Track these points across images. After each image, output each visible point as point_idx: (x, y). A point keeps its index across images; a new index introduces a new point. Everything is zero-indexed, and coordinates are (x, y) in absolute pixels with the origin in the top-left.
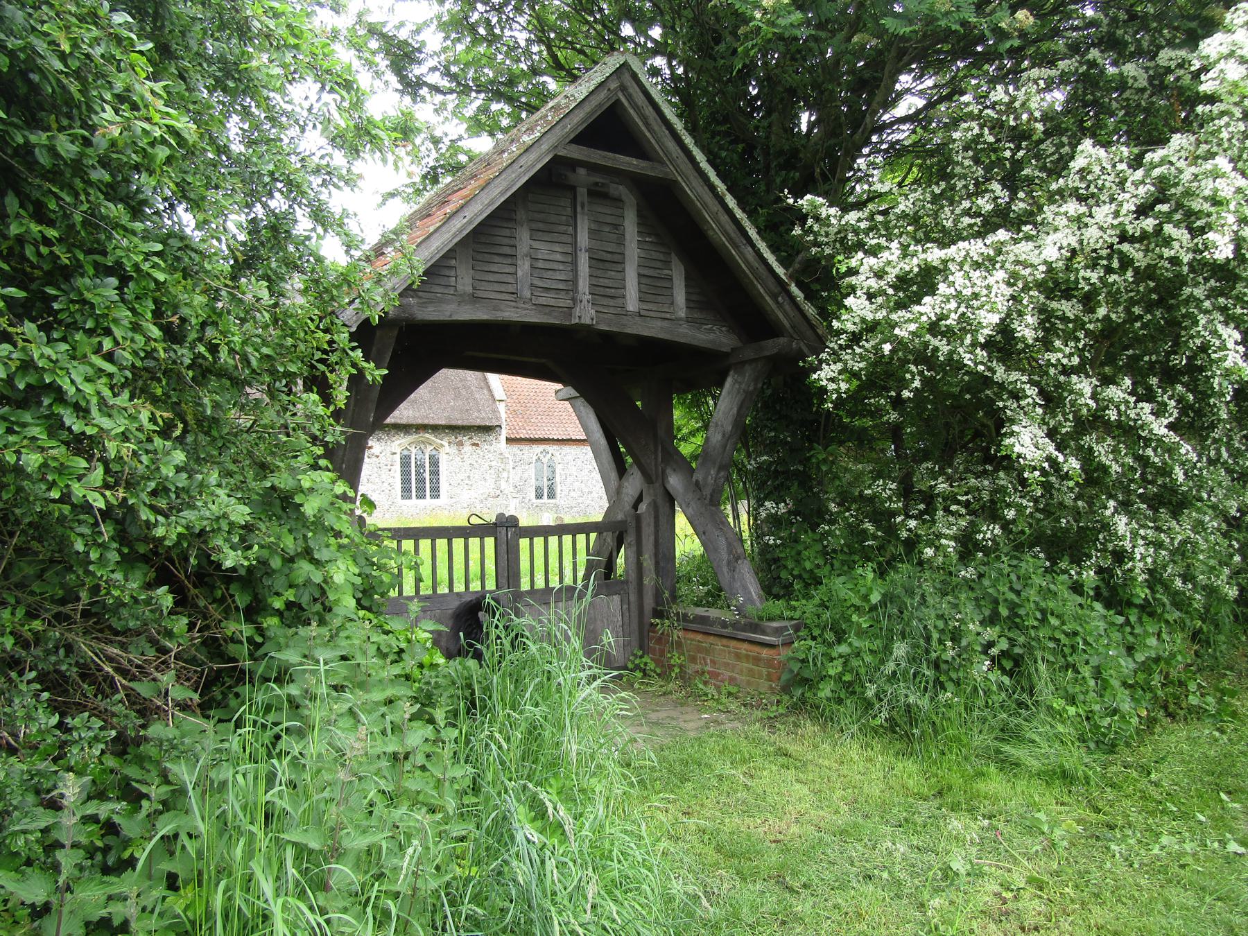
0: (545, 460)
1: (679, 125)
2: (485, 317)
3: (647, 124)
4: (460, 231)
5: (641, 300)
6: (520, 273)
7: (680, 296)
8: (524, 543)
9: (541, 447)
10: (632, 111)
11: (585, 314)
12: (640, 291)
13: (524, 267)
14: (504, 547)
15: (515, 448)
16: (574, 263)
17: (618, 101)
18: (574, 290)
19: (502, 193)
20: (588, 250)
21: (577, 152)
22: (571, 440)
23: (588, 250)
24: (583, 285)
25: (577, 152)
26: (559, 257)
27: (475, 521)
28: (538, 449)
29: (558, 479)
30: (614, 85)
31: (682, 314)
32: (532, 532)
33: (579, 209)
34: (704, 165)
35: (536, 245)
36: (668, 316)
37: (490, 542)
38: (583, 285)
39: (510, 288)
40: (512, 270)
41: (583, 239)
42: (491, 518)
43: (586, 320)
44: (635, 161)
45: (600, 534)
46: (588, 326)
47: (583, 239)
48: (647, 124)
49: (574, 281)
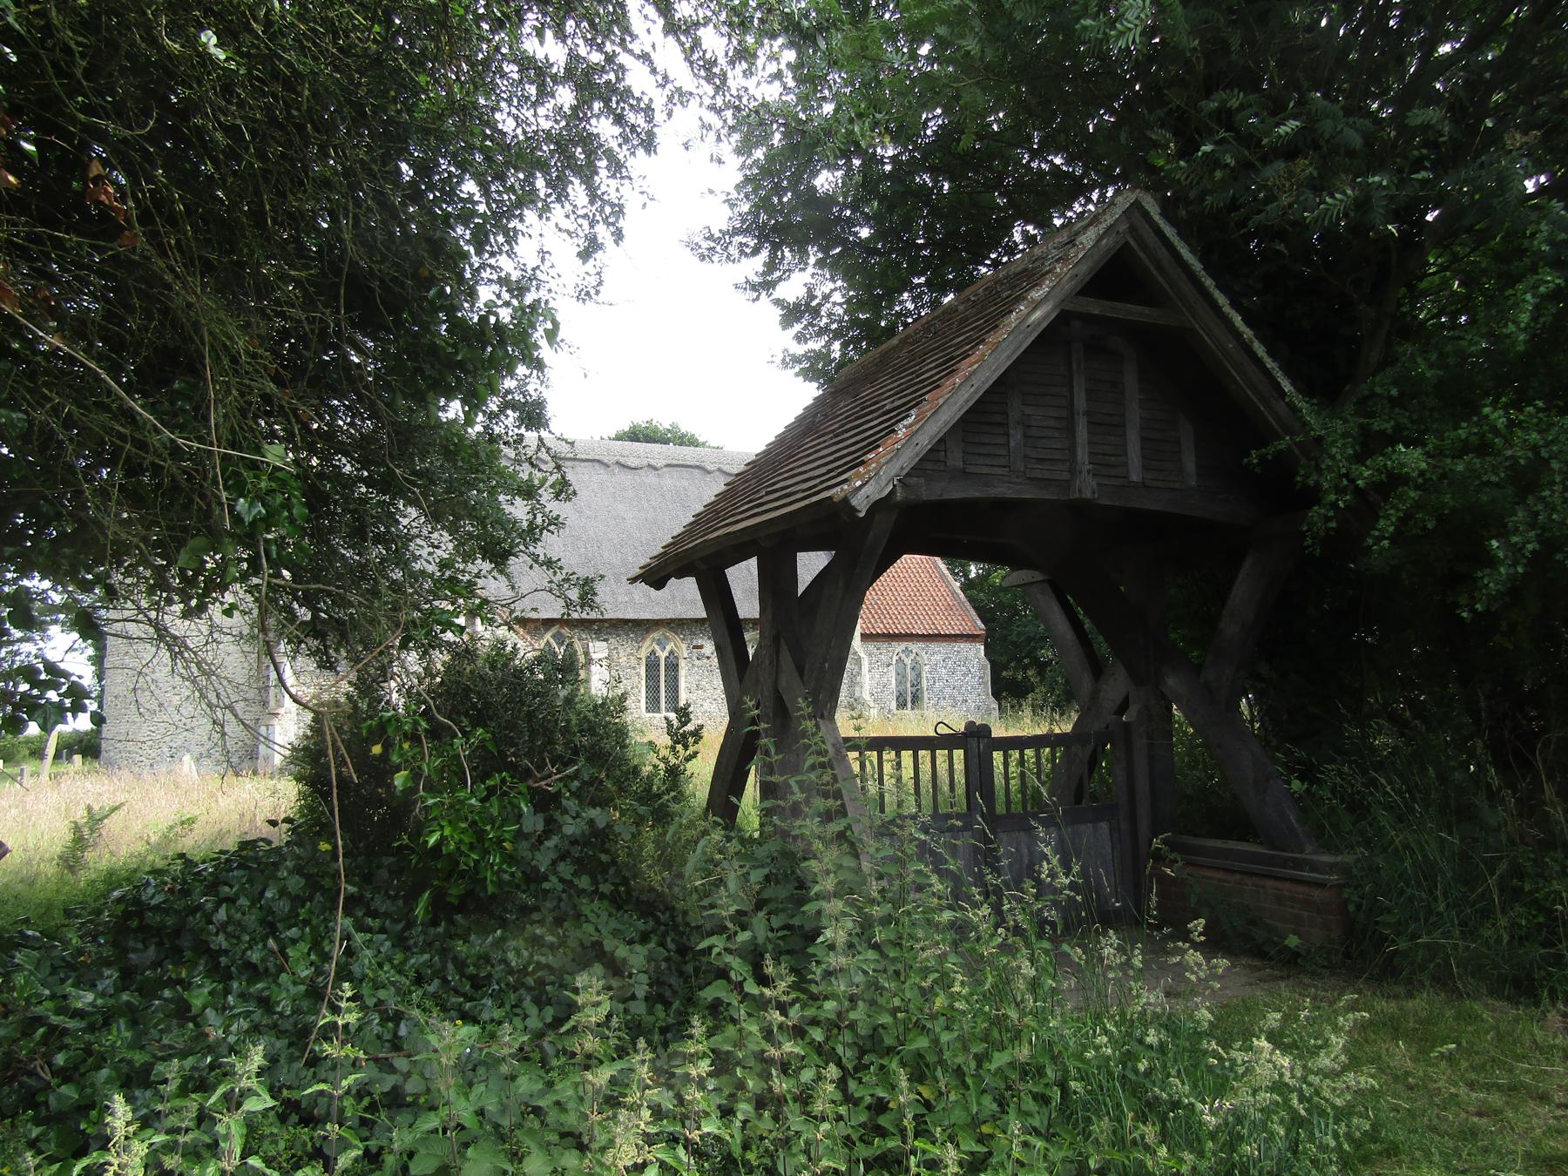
0: (908, 662)
1: (1197, 266)
2: (977, 494)
3: (1160, 268)
4: (967, 401)
5: (1145, 468)
6: (1012, 444)
7: (1190, 465)
8: (998, 756)
9: (903, 645)
10: (1141, 254)
11: (1087, 487)
12: (1144, 457)
13: (1016, 437)
14: (976, 760)
15: (871, 646)
16: (1070, 430)
17: (1127, 244)
18: (1073, 460)
19: (1008, 357)
20: (1087, 413)
21: (1095, 307)
22: (939, 635)
23: (1087, 413)
24: (1082, 454)
25: (1095, 307)
26: (1052, 423)
27: (943, 730)
28: (899, 647)
29: (925, 684)
30: (1123, 227)
31: (1193, 483)
32: (1007, 744)
33: (1074, 367)
34: (1227, 309)
35: (1028, 410)
36: (1177, 486)
37: (959, 754)
38: (1082, 454)
39: (1003, 462)
40: (1001, 440)
41: (1081, 402)
42: (960, 727)
43: (1088, 494)
44: (1147, 310)
45: (1068, 748)
46: (1088, 501)
47: (1081, 402)
48: (1160, 268)
49: (1072, 449)
